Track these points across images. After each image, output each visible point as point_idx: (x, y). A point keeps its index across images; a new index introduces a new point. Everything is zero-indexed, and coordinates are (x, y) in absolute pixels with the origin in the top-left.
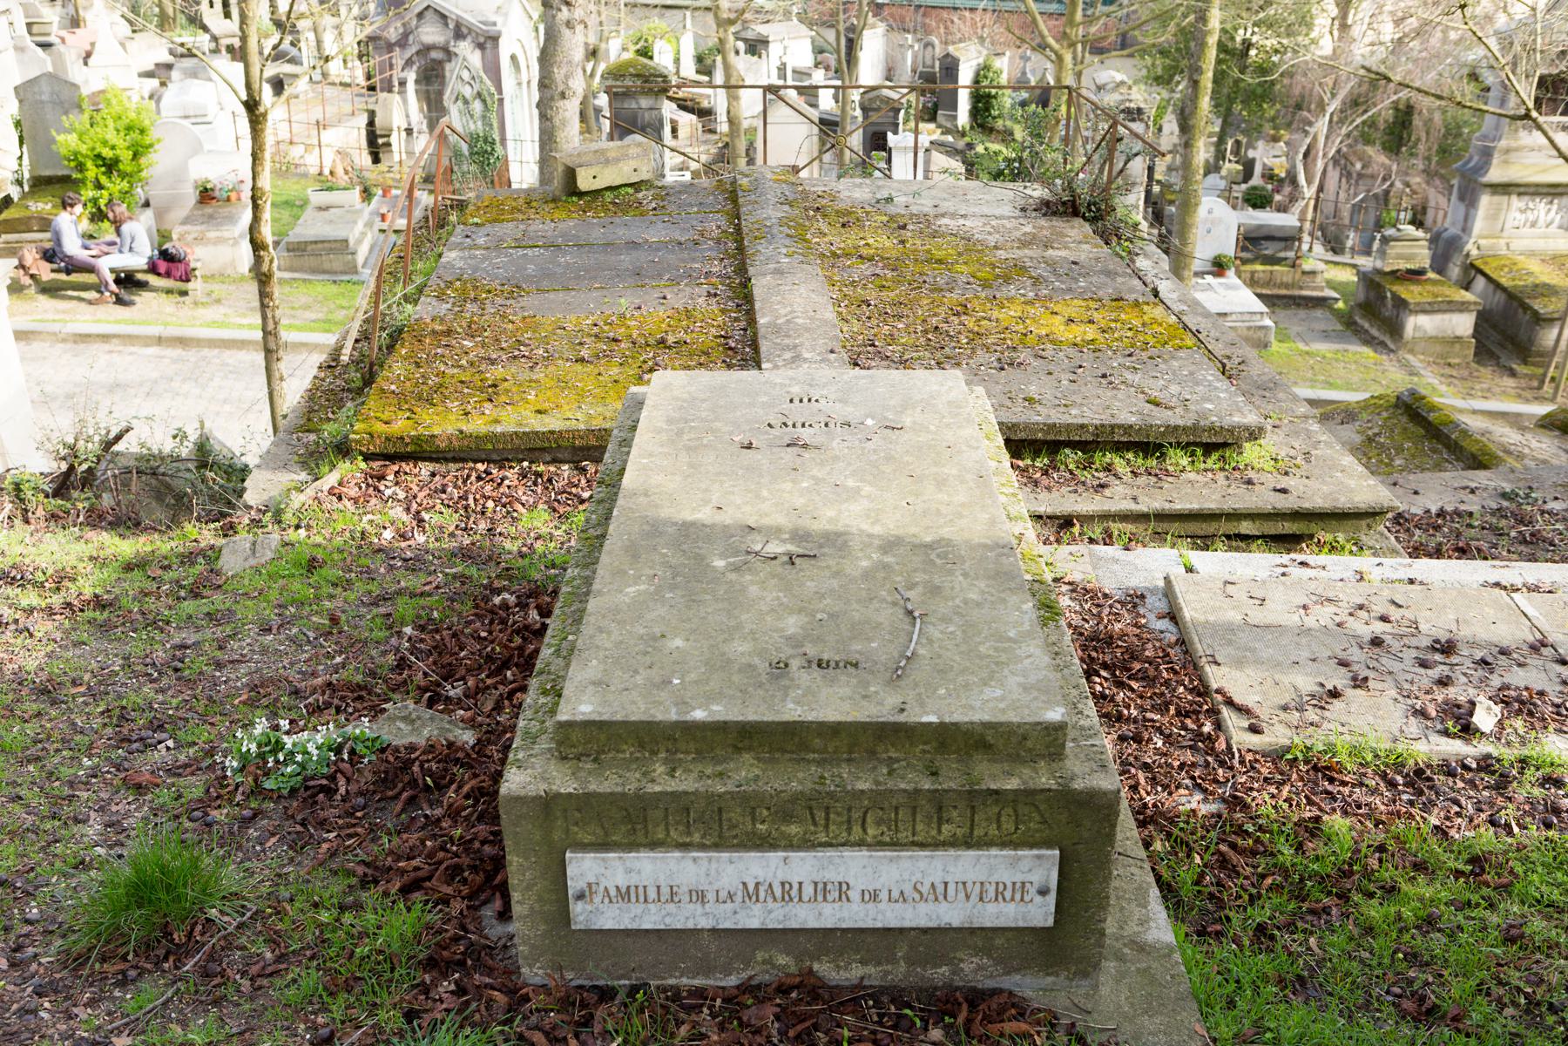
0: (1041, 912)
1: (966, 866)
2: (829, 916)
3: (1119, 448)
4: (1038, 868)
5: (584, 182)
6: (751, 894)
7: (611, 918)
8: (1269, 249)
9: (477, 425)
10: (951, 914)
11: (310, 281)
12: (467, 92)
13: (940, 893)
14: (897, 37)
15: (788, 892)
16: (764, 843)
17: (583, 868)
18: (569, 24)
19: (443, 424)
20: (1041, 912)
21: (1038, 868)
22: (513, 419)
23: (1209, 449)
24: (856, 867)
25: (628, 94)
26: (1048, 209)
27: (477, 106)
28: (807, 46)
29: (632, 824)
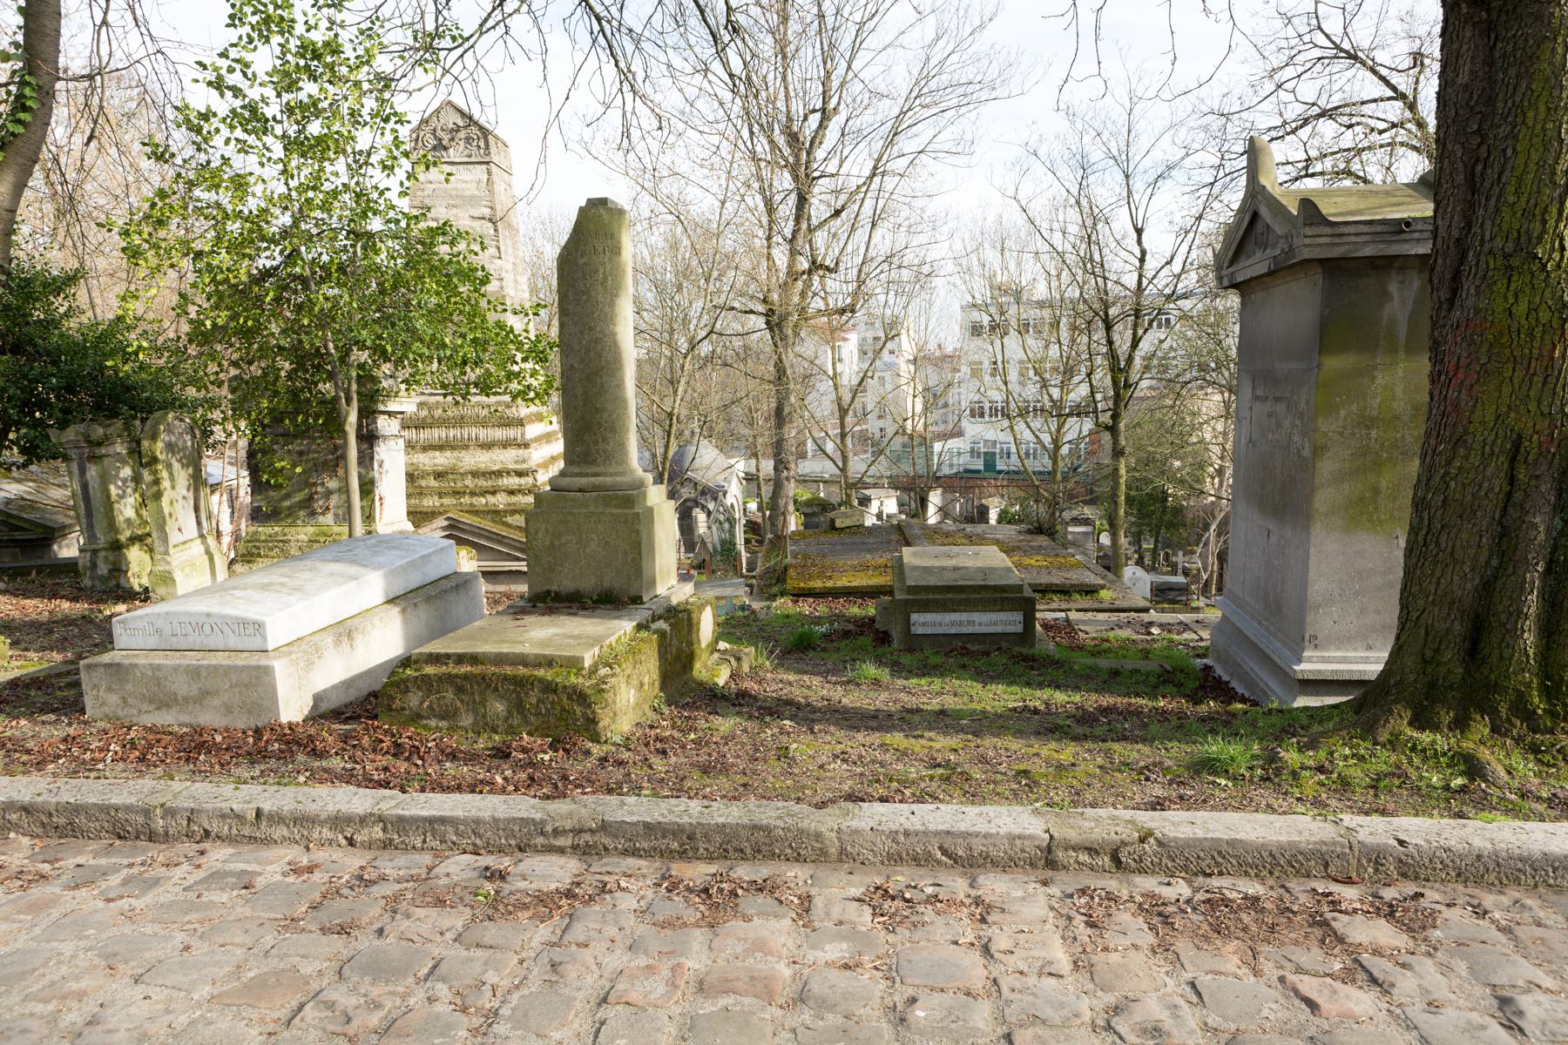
0: (1019, 628)
1: (1002, 616)
2: (970, 630)
3: (1054, 592)
4: (1018, 616)
5: (838, 524)
6: (952, 624)
7: (920, 631)
8: (1171, 595)
9: (830, 584)
10: (999, 629)
11: (198, 831)
12: (722, 518)
13: (995, 624)
14: (950, 497)
15: (961, 623)
16: (954, 611)
17: (914, 617)
18: (787, 479)
19: (818, 584)
20: (1019, 628)
21: (1018, 616)
22: (843, 582)
23: (1087, 593)
24: (977, 617)
25: (814, 514)
26: (1030, 532)
27: (726, 525)
28: (894, 501)
29: (926, 607)
